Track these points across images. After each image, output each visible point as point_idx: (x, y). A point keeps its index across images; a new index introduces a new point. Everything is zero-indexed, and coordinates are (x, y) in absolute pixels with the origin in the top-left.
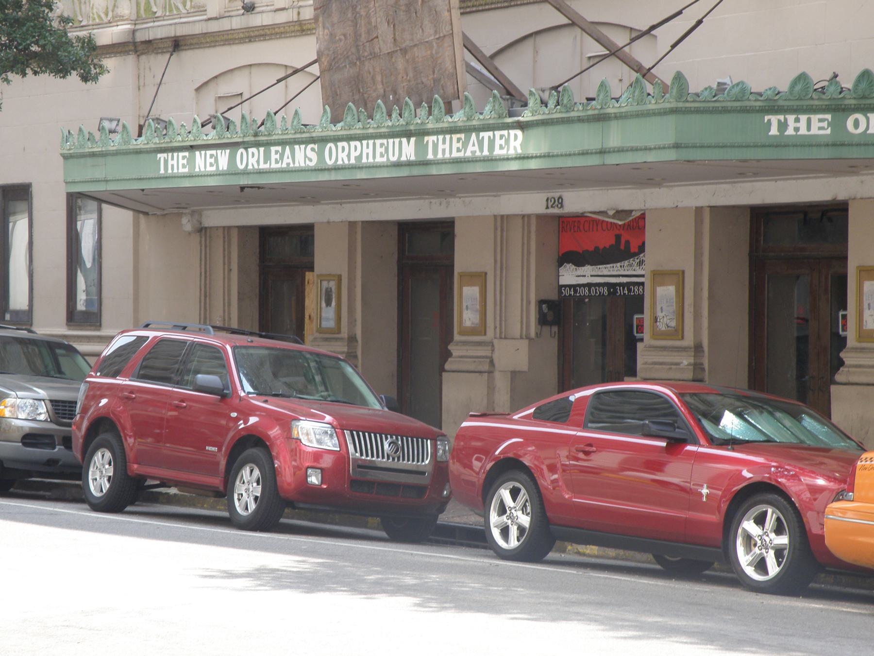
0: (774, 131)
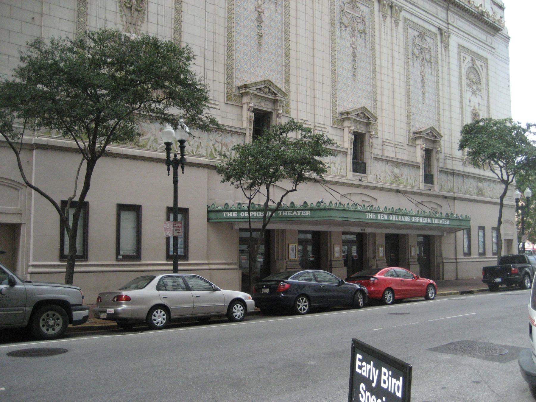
0: (280, 214)
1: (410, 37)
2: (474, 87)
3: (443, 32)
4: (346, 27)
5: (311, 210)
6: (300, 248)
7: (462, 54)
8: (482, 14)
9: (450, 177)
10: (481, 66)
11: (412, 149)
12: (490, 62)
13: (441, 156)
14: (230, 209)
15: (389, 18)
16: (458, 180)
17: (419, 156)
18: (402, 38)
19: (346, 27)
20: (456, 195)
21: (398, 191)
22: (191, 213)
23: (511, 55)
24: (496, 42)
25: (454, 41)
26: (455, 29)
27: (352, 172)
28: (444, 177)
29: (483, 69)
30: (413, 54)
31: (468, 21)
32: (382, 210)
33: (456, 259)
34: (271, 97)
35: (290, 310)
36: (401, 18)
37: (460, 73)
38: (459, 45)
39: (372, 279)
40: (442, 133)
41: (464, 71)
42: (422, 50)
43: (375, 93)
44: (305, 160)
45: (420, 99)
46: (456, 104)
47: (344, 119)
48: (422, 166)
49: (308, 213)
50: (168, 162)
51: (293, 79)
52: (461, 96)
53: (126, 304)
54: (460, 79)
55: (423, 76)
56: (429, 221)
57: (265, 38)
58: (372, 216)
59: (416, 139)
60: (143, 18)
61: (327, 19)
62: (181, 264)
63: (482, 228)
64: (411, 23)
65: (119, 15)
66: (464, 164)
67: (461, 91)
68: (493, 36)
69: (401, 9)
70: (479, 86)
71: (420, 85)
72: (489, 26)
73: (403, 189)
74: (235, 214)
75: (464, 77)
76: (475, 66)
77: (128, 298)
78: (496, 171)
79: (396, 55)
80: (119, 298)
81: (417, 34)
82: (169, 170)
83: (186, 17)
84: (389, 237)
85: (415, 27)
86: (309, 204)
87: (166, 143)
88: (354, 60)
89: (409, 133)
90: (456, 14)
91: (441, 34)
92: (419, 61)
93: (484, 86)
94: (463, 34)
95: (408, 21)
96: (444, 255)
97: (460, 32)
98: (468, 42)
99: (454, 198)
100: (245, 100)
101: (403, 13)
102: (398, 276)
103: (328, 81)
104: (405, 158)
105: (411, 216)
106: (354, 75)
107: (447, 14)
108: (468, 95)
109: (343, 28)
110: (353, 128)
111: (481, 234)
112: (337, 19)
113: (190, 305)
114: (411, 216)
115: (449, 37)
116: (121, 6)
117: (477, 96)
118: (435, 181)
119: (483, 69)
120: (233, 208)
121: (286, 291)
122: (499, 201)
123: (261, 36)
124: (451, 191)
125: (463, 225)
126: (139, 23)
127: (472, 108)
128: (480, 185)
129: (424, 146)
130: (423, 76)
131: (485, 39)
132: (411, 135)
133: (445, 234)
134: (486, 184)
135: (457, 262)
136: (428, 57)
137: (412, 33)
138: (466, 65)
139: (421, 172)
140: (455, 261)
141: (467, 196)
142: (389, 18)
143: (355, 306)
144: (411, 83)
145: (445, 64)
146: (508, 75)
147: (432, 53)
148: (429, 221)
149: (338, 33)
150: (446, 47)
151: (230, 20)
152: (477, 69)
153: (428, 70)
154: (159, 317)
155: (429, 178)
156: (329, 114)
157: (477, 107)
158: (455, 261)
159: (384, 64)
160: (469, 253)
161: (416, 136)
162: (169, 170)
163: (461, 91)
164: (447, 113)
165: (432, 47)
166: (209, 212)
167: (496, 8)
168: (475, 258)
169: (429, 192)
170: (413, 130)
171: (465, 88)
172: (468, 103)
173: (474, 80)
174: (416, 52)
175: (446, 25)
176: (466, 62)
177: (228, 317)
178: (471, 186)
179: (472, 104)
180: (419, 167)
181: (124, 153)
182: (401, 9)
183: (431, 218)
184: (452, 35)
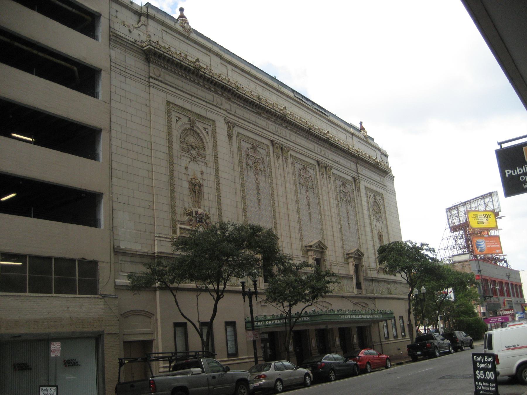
1: (338, 186)
2: (194, 153)
3: (274, 142)
4: (251, 167)
5: (310, 316)
6: (262, 345)
7: (368, 193)
8: (378, 164)
9: (371, 283)
10: (205, 129)
11: (346, 266)
12: (384, 196)
13: (364, 268)
14: (259, 319)
15: (325, 176)
16: (375, 284)
17: (352, 271)
18: (291, 171)
19: (303, 185)
20: (376, 295)
21: (342, 297)
23: (396, 189)
24: (386, 180)
25: (363, 184)
26: (362, 177)
27: (263, 283)
28: (367, 283)
29: (208, 132)
30: (341, 198)
31: (369, 169)
32: (347, 312)
33: (381, 342)
34: (320, 250)
35: (327, 379)
36: (234, 133)
38: (366, 188)
39: (357, 357)
40: (326, 244)
41: (370, 205)
42: (345, 194)
43: (322, 229)
44: (317, 284)
45: (348, 229)
46: (368, 230)
47: (308, 251)
48: (354, 277)
49: (308, 318)
50: (244, 293)
51: (278, 227)
52: (371, 224)
53: (265, 379)
55: (348, 213)
56: (371, 316)
57: (262, 201)
58: (342, 317)
59: (348, 258)
60: (201, 197)
61: (292, 182)
62: (252, 358)
64: (244, 137)
65: (190, 197)
66: (378, 273)
68: (384, 177)
69: (331, 168)
70: (201, 151)
71: (346, 219)
72: (335, 147)
73: (346, 295)
74: (262, 323)
75: (371, 210)
76: (195, 128)
77: (265, 376)
78: (401, 277)
79: (331, 200)
80: (260, 377)
81: (341, 183)
82: (244, 298)
83: (223, 194)
84: (358, 328)
85: (340, 178)
86: (308, 313)
87: (241, 282)
88: (258, 193)
89: (302, 247)
91: (355, 181)
92: (344, 202)
93: (383, 214)
94: (368, 179)
95: (171, 106)
96: (373, 340)
97: (193, 98)
98: (183, 100)
99: (375, 298)
100: (310, 253)
101: (291, 152)
102: (335, 360)
103: (297, 225)
104: (344, 273)
105: (362, 314)
106: (310, 219)
107: (357, 166)
108: (375, 222)
109: (249, 169)
110: (315, 256)
111: (401, 321)
112: (244, 161)
113: (289, 378)
114: (362, 314)
115: (359, 182)
116: (190, 191)
117: (198, 162)
118: (363, 287)
119: (208, 132)
120: (261, 319)
121: (322, 368)
122: (407, 297)
123: (259, 200)
124: (373, 293)
125: (388, 316)
126: (200, 201)
128: (389, 286)
129: (355, 263)
130: (348, 213)
131: (212, 100)
132: (304, 248)
133: (373, 325)
134: (392, 285)
135: (381, 344)
136: (349, 198)
137: (245, 145)
138: (371, 200)
139: (354, 282)
140: (379, 343)
141: (383, 296)
142: (325, 176)
143: (355, 375)
144: (342, 218)
145: (359, 202)
146: (396, 203)
147: (265, 162)
148: (371, 316)
149: (299, 191)
150: (359, 190)
151: (243, 191)
152: (200, 132)
153: (350, 208)
154: (279, 386)
155: (359, 286)
156: (299, 248)
157: (199, 176)
158: (379, 343)
159: (326, 208)
160: (388, 338)
161: (348, 256)
162: (244, 298)
164: (364, 237)
165: (313, 176)
166: (246, 323)
167: (383, 157)
169: (360, 295)
170: (346, 252)
171: (372, 217)
173: (193, 144)
174: (250, 162)
175: (357, 174)
177: (302, 384)
178: (383, 287)
179: (378, 228)
180: (352, 278)
181: (237, 290)
182: (331, 168)
183: (372, 314)
184: (361, 181)
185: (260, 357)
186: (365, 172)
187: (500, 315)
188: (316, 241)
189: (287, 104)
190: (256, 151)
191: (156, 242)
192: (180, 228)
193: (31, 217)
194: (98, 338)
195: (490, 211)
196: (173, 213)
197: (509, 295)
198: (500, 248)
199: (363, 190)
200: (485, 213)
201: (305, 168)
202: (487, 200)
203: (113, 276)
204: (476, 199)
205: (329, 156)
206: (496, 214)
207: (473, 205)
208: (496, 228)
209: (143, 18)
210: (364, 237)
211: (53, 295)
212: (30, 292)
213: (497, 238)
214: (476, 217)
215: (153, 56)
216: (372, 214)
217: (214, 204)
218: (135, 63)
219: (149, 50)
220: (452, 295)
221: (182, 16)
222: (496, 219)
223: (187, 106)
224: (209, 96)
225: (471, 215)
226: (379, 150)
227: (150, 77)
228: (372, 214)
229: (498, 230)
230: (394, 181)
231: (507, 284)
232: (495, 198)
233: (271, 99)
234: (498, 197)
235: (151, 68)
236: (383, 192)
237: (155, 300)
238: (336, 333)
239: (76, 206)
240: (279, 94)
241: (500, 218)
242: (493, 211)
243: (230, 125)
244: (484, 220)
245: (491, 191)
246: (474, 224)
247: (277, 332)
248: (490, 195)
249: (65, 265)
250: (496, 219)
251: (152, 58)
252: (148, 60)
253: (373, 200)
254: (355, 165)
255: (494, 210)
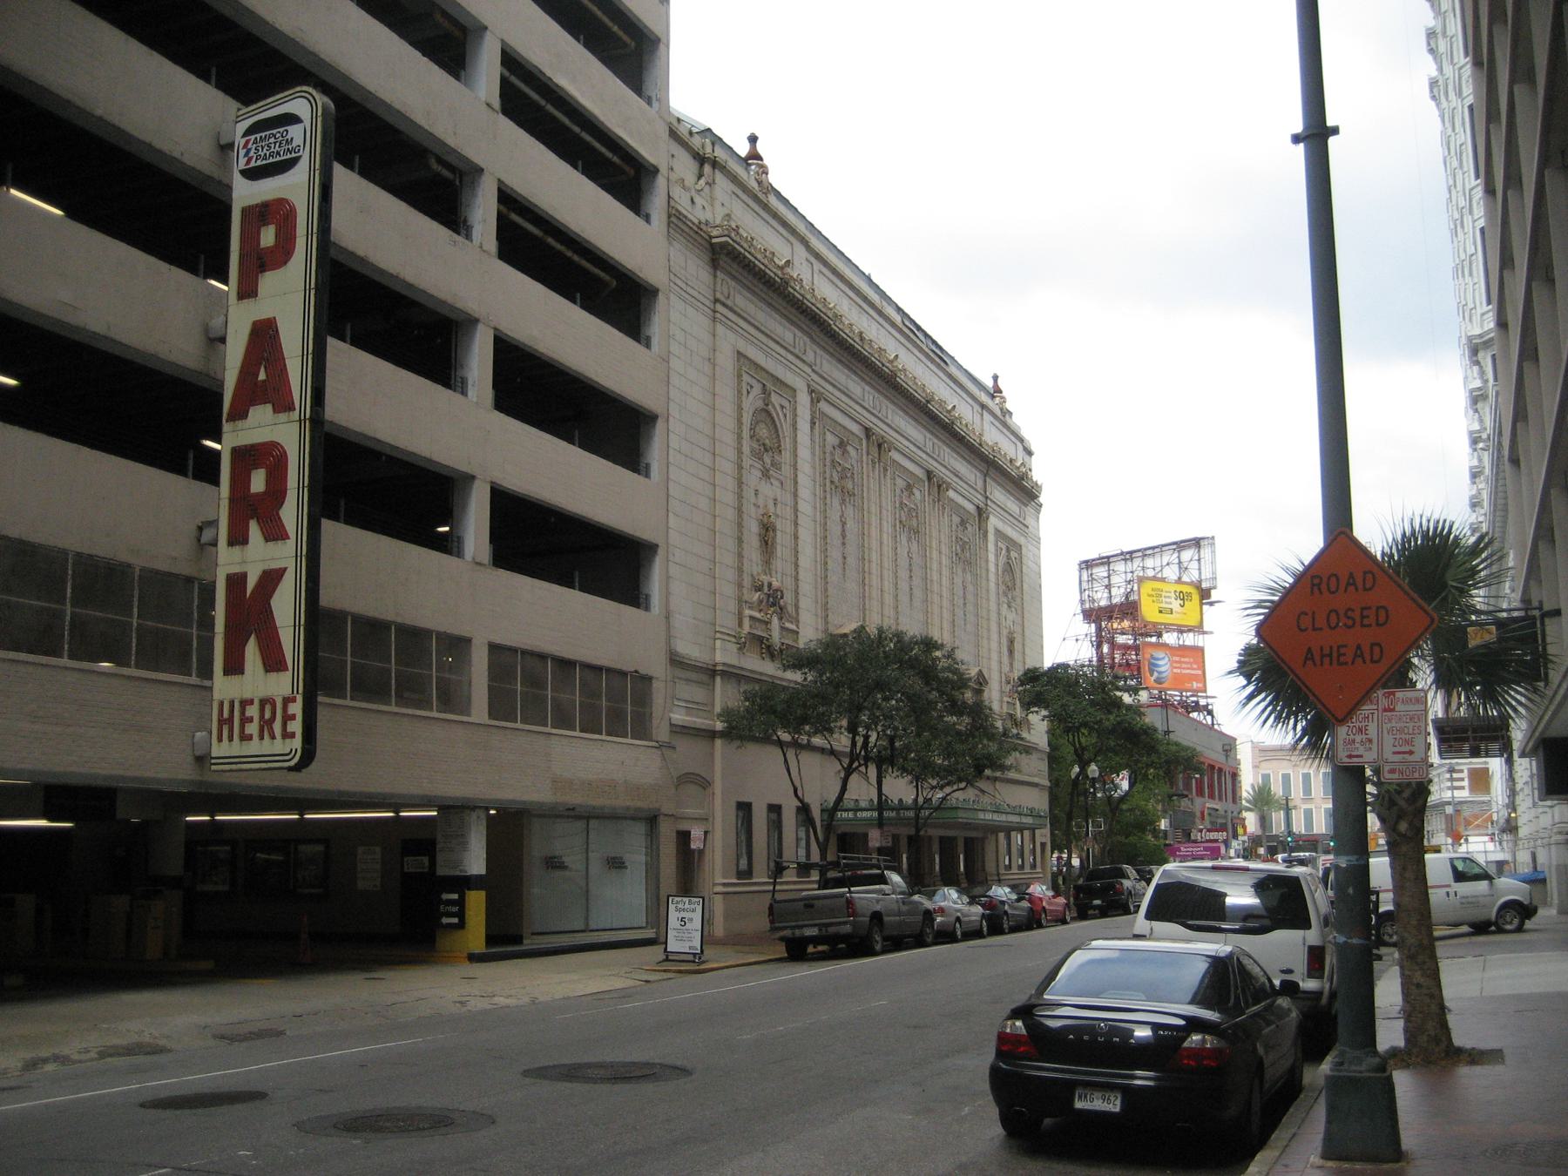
1: (829, 449)
7: (746, 378)
22: (755, 809)
24: (1030, 510)
25: (993, 522)
31: (754, 293)
37: (740, 423)
46: (994, 627)
54: (740, 437)
63: (775, 809)
67: (740, 467)
72: (755, 275)
74: (851, 815)
75: (746, 434)
81: (836, 441)
90: (734, 278)
93: (786, 456)
108: (753, 477)
127: (761, 511)
136: (850, 486)
138: (752, 402)
143: (869, 952)
153: (850, 511)
163: (740, 467)
168: (787, 883)
171: (747, 462)
172: (753, 499)
176: (751, 396)
185: (1379, 853)
186: (998, 495)
187: (1195, 842)
188: (854, 626)
189: (902, 353)
190: (845, 452)
191: (718, 643)
192: (751, 618)
193: (186, 475)
194: (652, 820)
195: (1191, 584)
196: (740, 586)
197: (1211, 796)
198: (1203, 678)
199: (991, 537)
200: (1179, 588)
201: (909, 487)
202: (1187, 555)
203: (674, 706)
204: (1160, 548)
205: (953, 464)
206: (1205, 594)
207: (1149, 562)
208: (1198, 629)
209: (707, 168)
210: (985, 641)
211: (65, 661)
212: (71, 657)
213: (1198, 652)
214: (1157, 595)
215: (727, 256)
216: (746, 449)
217: (789, 569)
218: (694, 269)
219: (723, 246)
220: (1125, 785)
221: (755, 156)
222: (1202, 604)
223: (760, 359)
224: (787, 333)
225: (1147, 588)
226: (1022, 440)
227: (716, 301)
228: (746, 449)
229: (1204, 633)
230: (1041, 516)
231: (1220, 770)
232: (1206, 552)
233: (826, 293)
234: (1213, 552)
235: (719, 281)
236: (1022, 541)
237: (712, 755)
238: (936, 847)
239: (607, 562)
240: (881, 320)
241: (1211, 604)
242: (1197, 585)
243: (816, 396)
244: (1176, 605)
245: (1199, 535)
246: (1149, 612)
247: (854, 834)
248: (1197, 543)
249: (103, 579)
250: (1202, 604)
251: (724, 260)
252: (714, 264)
253: (760, 404)
254: (966, 463)
255: (1200, 582)
